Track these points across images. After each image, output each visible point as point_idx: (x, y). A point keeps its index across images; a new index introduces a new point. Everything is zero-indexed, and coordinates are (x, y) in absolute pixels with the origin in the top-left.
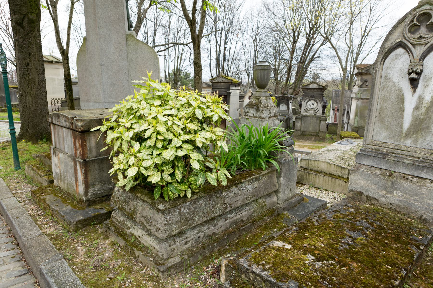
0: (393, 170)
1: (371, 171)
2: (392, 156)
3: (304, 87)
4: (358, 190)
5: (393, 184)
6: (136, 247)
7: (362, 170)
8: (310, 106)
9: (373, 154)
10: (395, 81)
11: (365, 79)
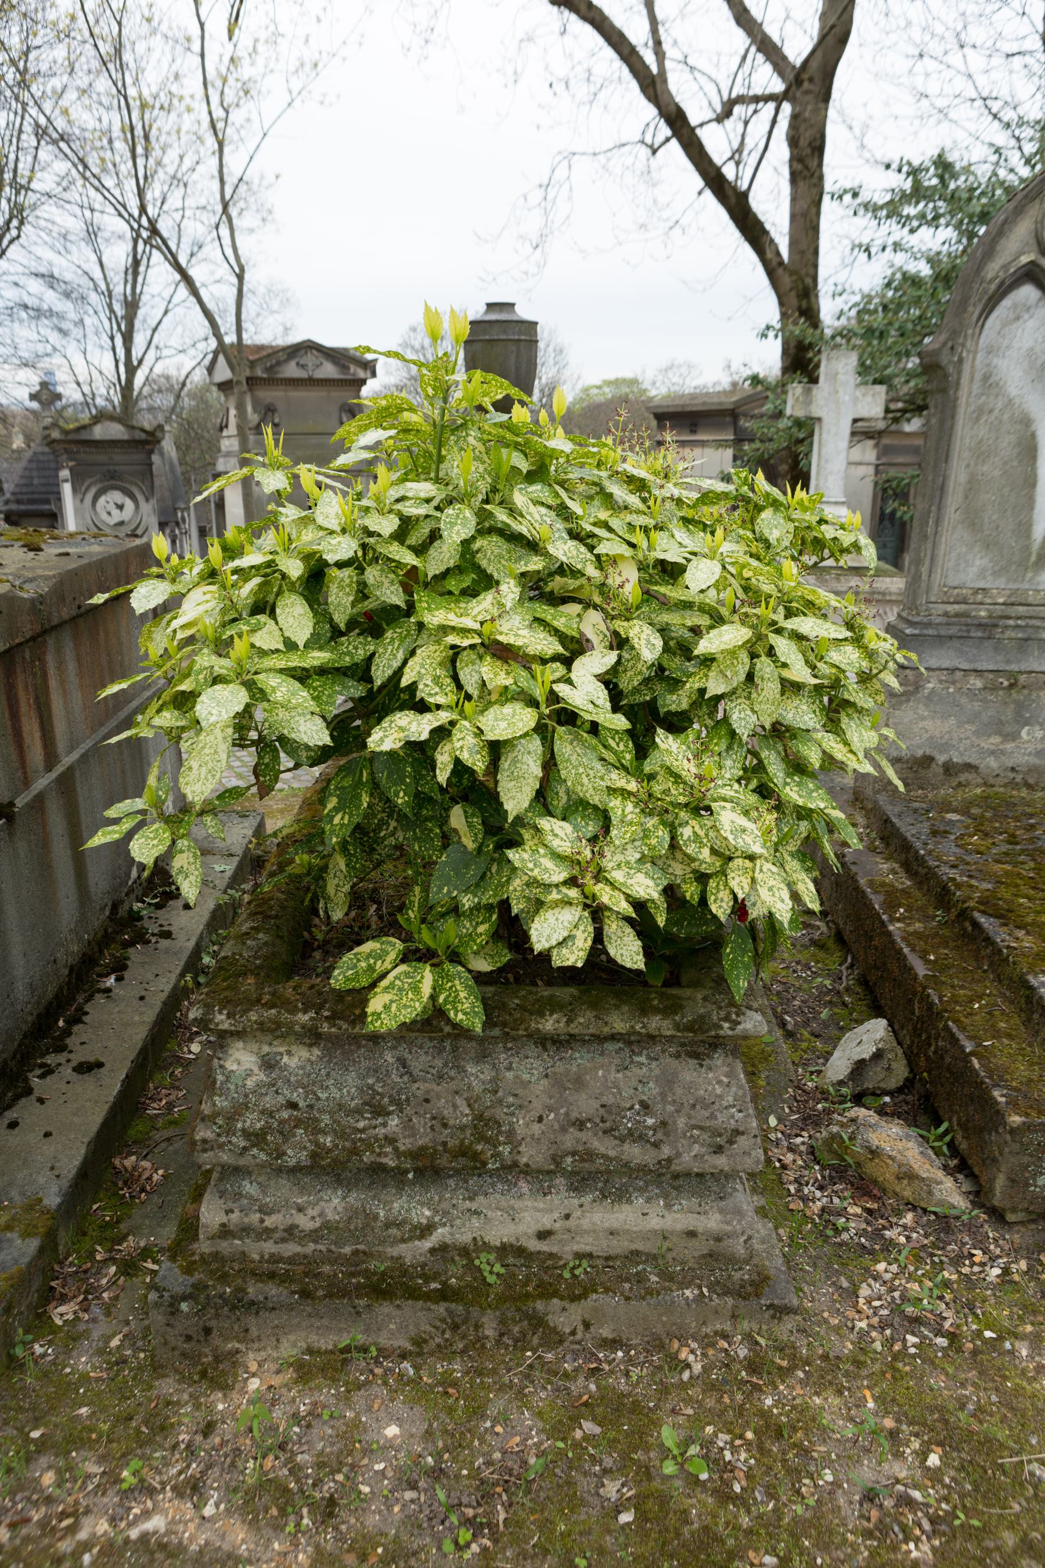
0: (1014, 667)
1: (959, 685)
2: (1007, 627)
3: (71, 437)
4: (920, 753)
5: (1020, 707)
6: (547, 1291)
7: (930, 685)
8: (109, 513)
9: (953, 631)
10: (1013, 390)
11: (268, 401)
